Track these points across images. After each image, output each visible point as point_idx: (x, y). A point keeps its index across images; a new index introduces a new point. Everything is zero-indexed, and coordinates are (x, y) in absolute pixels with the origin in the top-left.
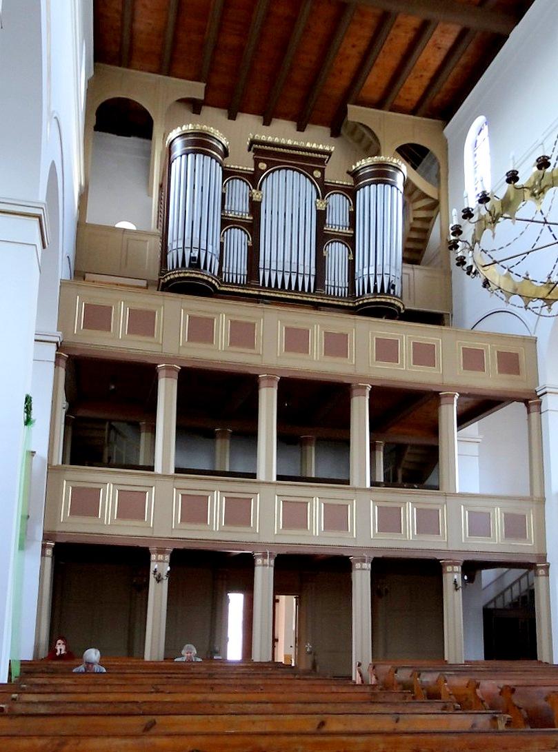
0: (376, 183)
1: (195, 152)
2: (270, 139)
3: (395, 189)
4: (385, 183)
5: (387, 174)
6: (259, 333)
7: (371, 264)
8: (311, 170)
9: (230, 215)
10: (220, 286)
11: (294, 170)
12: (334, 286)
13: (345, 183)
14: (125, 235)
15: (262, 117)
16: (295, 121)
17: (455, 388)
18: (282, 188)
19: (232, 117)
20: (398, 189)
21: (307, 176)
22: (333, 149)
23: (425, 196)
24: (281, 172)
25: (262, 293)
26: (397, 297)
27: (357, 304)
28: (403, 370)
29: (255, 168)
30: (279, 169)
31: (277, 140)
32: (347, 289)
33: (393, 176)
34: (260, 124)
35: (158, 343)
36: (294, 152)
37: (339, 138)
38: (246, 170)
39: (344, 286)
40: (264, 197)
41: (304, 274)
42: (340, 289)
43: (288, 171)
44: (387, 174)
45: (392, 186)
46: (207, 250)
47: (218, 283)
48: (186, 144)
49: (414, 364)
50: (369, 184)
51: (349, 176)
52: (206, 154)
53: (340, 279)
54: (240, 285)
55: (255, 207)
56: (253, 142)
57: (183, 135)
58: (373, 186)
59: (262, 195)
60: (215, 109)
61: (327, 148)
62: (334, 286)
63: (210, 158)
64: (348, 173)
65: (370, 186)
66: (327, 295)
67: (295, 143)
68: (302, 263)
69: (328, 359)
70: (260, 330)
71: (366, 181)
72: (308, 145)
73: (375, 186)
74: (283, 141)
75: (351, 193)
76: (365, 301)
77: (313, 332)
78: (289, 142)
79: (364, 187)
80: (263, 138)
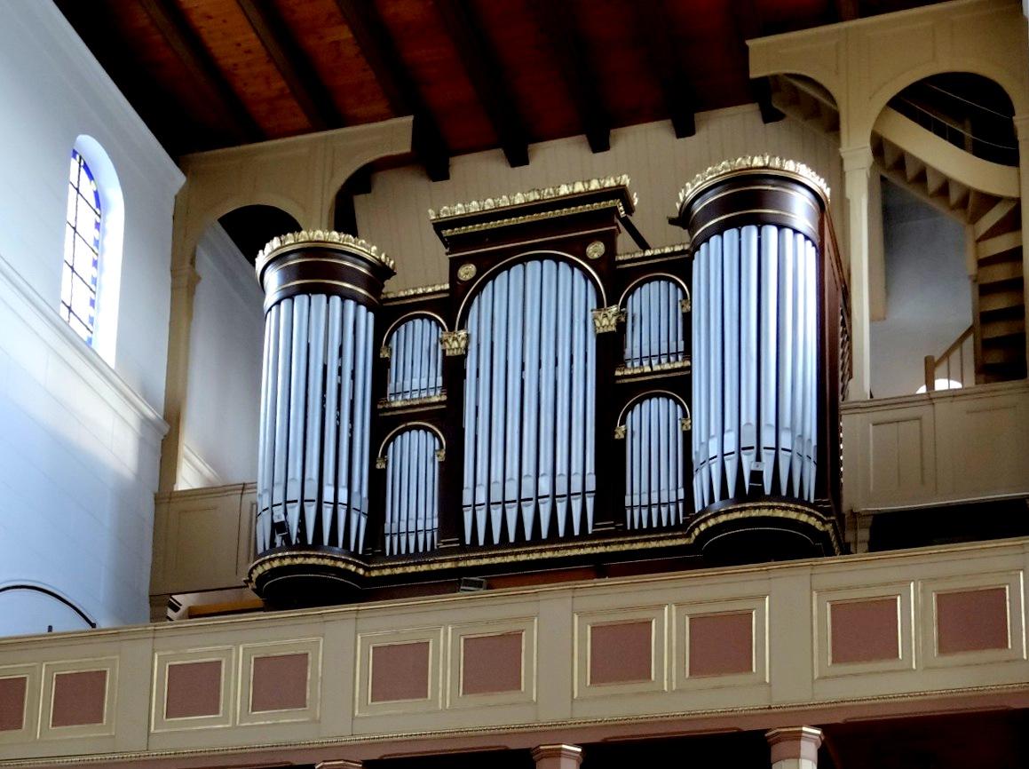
0: (737, 223)
1: (303, 290)
2: (474, 207)
3: (788, 232)
4: (760, 222)
5: (759, 199)
6: (315, 673)
7: (727, 426)
8: (579, 247)
9: (398, 404)
10: (688, 536)
11: (541, 258)
12: (650, 506)
13: (667, 250)
14: (245, 497)
15: (668, 122)
16: (608, 134)
17: (804, 714)
18: (516, 309)
19: (684, 129)
20: (796, 232)
21: (573, 264)
22: (625, 180)
23: (989, 201)
24: (513, 270)
25: (462, 564)
26: (807, 504)
27: (375, 574)
28: (229, 728)
29: (451, 283)
30: (508, 267)
31: (489, 204)
32: (681, 505)
33: (778, 201)
34: (586, 153)
35: (530, 702)
36: (535, 217)
37: (785, 120)
38: (434, 293)
39: (673, 499)
40: (473, 347)
41: (569, 494)
42: (664, 510)
43: (530, 265)
44: (302, 271)
45: (781, 227)
46: (349, 504)
47: (819, 518)
48: (288, 274)
49: (217, 713)
50: (720, 230)
51: (678, 229)
52: (330, 291)
53: (663, 485)
54: (669, 528)
55: (454, 370)
56: (439, 226)
57: (277, 259)
58: (730, 234)
59: (468, 337)
60: (475, 155)
61: (610, 183)
62: (399, 534)
63: (324, 297)
64: (672, 221)
65: (721, 234)
66: (633, 532)
67: (532, 198)
68: (565, 472)
69: (475, 700)
70: (316, 669)
71: (707, 225)
72: (564, 190)
73: (719, 238)
74: (504, 202)
75: (679, 268)
76: (711, 522)
77: (437, 645)
78: (519, 199)
79: (707, 240)
80: (459, 210)
